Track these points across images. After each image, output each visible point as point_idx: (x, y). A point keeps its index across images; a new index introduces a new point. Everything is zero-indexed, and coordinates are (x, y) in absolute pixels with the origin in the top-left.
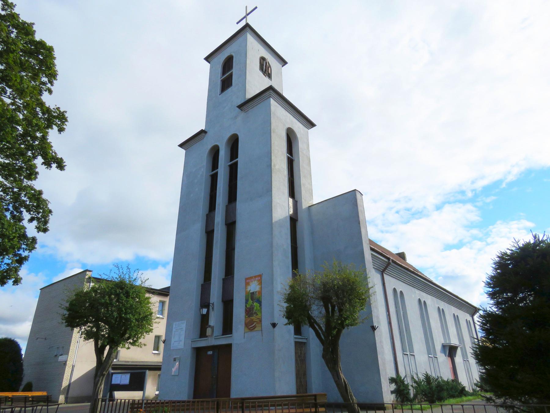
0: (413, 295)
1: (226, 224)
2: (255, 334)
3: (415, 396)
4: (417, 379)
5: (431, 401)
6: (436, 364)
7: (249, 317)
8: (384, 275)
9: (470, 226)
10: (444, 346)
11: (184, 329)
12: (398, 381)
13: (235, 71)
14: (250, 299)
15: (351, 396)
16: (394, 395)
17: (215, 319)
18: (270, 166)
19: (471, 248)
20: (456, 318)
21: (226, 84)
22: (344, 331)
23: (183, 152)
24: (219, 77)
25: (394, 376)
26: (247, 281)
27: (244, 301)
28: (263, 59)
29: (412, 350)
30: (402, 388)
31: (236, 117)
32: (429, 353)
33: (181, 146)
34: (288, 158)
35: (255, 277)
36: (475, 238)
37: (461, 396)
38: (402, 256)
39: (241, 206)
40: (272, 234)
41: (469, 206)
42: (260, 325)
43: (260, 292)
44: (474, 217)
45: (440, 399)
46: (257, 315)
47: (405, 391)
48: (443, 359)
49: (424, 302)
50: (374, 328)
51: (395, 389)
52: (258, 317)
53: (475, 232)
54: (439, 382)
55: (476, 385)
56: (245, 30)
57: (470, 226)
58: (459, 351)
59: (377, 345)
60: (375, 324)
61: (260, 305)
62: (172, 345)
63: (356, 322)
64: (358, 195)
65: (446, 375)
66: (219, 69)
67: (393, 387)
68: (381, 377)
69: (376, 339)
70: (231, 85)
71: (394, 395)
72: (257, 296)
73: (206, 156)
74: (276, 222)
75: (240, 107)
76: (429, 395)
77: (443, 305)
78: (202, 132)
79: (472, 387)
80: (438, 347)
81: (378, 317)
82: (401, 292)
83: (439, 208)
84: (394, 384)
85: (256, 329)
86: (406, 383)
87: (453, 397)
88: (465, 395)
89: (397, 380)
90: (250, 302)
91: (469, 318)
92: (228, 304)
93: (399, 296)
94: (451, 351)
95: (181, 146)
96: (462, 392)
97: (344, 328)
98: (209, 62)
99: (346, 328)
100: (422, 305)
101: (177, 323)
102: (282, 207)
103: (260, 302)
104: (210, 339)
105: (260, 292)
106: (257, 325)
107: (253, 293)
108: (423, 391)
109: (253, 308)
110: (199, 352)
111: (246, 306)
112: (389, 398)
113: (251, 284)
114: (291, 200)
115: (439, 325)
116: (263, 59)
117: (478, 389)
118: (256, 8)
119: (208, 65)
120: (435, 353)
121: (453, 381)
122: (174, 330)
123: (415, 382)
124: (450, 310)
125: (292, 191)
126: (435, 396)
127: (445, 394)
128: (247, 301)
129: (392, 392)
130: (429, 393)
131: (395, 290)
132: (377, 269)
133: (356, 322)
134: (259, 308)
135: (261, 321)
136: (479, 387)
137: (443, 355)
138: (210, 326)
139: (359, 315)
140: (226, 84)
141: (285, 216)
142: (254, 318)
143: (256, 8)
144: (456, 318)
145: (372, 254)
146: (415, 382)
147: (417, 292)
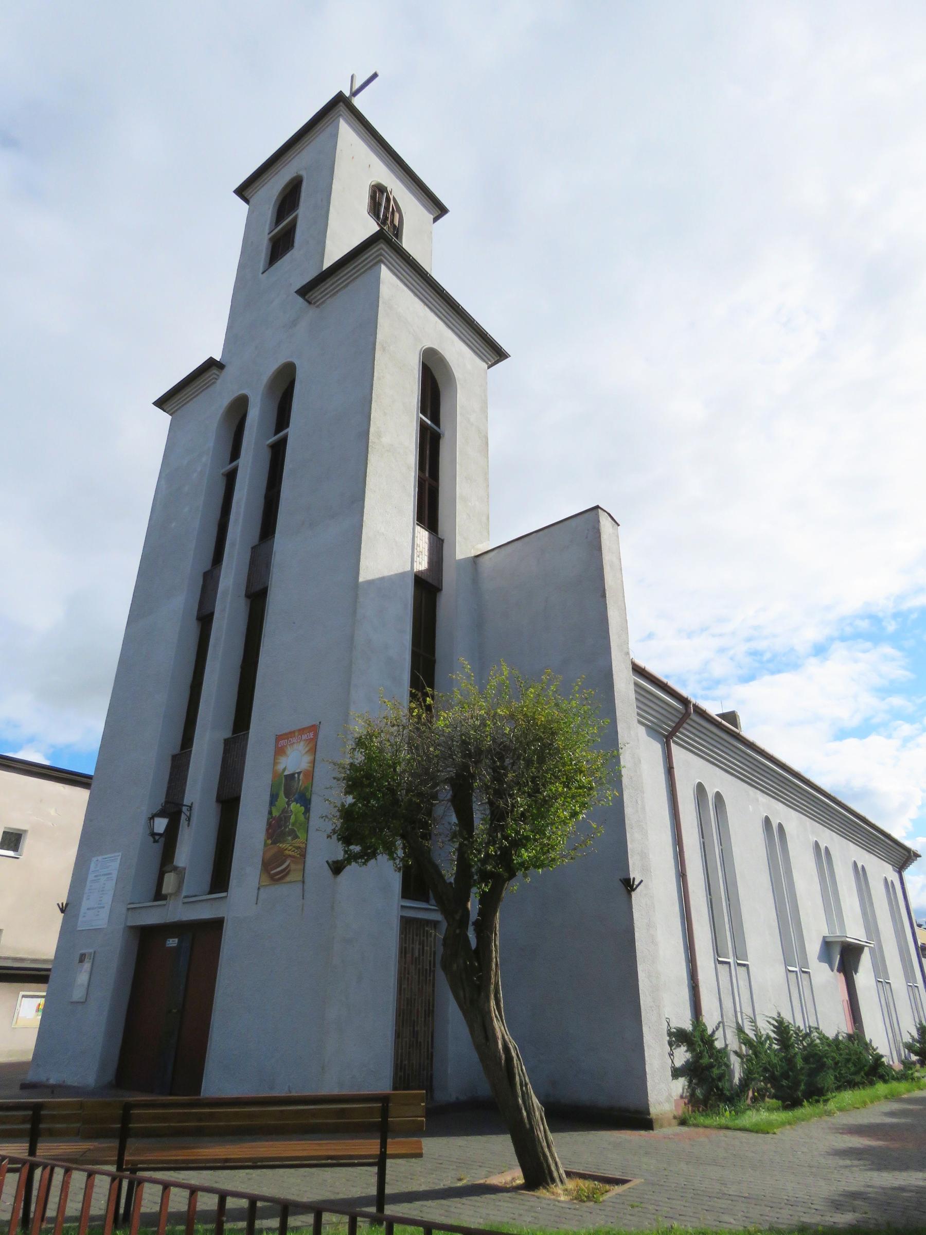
0: (748, 807)
1: (248, 596)
2: (286, 891)
3: (745, 1083)
4: (751, 1035)
5: (791, 1102)
6: (807, 992)
7: (274, 843)
8: (672, 744)
9: (886, 690)
10: (827, 945)
11: (114, 876)
12: (697, 1039)
13: (304, 212)
14: (282, 794)
15: (525, 1096)
16: (681, 1084)
17: (193, 849)
18: (364, 435)
19: (889, 737)
20: (860, 873)
21: (281, 244)
22: (513, 887)
23: (164, 419)
24: (267, 230)
25: (688, 1026)
26: (282, 743)
27: (267, 798)
28: (378, 191)
29: (740, 952)
30: (705, 1061)
31: (294, 323)
32: (787, 962)
33: (161, 403)
34: (423, 428)
35: (302, 731)
36: (898, 715)
37: (872, 1083)
38: (731, 717)
39: (284, 544)
40: (355, 612)
41: (887, 649)
42: (300, 867)
43: (310, 774)
44: (897, 671)
45: (816, 1094)
46: (296, 837)
47: (716, 1072)
48: (825, 977)
49: (780, 826)
50: (629, 885)
51: (687, 1062)
52: (297, 843)
53: (897, 701)
54: (812, 1044)
55: (910, 1047)
56: (333, 114)
57: (886, 690)
58: (866, 959)
59: (637, 935)
60: (635, 874)
61: (307, 810)
62: (80, 919)
63: (552, 855)
64: (605, 523)
65: (833, 1023)
66: (268, 210)
67: (682, 1056)
68: (645, 1030)
69: (636, 915)
70: (293, 246)
71: (681, 1084)
72: (301, 783)
73: (216, 425)
74: (370, 583)
75: (304, 292)
76: (784, 1083)
77: (829, 839)
78: (210, 365)
79: (899, 1055)
80: (813, 948)
81: (644, 856)
82: (718, 796)
83: (820, 650)
84: (683, 1048)
85: (288, 879)
86: (719, 1044)
87: (852, 1085)
88: (884, 1079)
89: (695, 1038)
90: (282, 800)
91: (893, 876)
92: (228, 804)
93: (712, 807)
94: (846, 957)
95: (161, 403)
96: (871, 1071)
97: (512, 875)
98: (247, 201)
99: (520, 874)
100: (774, 834)
101: (100, 858)
102: (391, 545)
103: (305, 801)
104: (171, 902)
105: (310, 774)
106: (293, 867)
107: (291, 777)
108: (766, 1070)
109: (287, 819)
110: (146, 939)
111: (270, 813)
112: (665, 1091)
113: (289, 750)
114: (423, 536)
115: (817, 887)
116: (378, 191)
117: (914, 1058)
118: (375, 76)
119: (242, 208)
120: (805, 962)
121: (850, 1037)
122: (91, 877)
123: (747, 1042)
124: (846, 853)
125: (429, 509)
126: (802, 1087)
127: (829, 1079)
128: (274, 798)
129: (676, 1073)
130: (785, 1076)
131: (700, 789)
132: (653, 731)
133: (552, 855)
134: (302, 818)
135: (303, 855)
136: (916, 1054)
137: (825, 966)
138: (175, 869)
139: (563, 832)
140: (281, 244)
141: (401, 570)
142: (286, 846)
143: (375, 76)
144: (860, 873)
145: (636, 684)
146: (747, 1042)
147: (763, 799)
